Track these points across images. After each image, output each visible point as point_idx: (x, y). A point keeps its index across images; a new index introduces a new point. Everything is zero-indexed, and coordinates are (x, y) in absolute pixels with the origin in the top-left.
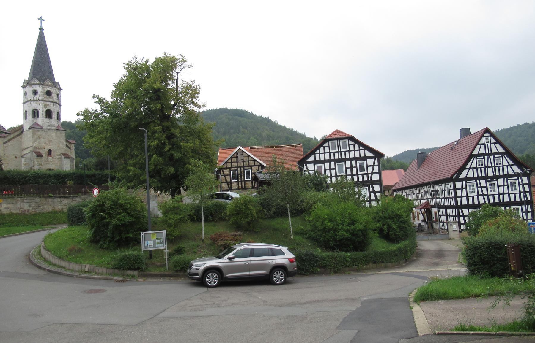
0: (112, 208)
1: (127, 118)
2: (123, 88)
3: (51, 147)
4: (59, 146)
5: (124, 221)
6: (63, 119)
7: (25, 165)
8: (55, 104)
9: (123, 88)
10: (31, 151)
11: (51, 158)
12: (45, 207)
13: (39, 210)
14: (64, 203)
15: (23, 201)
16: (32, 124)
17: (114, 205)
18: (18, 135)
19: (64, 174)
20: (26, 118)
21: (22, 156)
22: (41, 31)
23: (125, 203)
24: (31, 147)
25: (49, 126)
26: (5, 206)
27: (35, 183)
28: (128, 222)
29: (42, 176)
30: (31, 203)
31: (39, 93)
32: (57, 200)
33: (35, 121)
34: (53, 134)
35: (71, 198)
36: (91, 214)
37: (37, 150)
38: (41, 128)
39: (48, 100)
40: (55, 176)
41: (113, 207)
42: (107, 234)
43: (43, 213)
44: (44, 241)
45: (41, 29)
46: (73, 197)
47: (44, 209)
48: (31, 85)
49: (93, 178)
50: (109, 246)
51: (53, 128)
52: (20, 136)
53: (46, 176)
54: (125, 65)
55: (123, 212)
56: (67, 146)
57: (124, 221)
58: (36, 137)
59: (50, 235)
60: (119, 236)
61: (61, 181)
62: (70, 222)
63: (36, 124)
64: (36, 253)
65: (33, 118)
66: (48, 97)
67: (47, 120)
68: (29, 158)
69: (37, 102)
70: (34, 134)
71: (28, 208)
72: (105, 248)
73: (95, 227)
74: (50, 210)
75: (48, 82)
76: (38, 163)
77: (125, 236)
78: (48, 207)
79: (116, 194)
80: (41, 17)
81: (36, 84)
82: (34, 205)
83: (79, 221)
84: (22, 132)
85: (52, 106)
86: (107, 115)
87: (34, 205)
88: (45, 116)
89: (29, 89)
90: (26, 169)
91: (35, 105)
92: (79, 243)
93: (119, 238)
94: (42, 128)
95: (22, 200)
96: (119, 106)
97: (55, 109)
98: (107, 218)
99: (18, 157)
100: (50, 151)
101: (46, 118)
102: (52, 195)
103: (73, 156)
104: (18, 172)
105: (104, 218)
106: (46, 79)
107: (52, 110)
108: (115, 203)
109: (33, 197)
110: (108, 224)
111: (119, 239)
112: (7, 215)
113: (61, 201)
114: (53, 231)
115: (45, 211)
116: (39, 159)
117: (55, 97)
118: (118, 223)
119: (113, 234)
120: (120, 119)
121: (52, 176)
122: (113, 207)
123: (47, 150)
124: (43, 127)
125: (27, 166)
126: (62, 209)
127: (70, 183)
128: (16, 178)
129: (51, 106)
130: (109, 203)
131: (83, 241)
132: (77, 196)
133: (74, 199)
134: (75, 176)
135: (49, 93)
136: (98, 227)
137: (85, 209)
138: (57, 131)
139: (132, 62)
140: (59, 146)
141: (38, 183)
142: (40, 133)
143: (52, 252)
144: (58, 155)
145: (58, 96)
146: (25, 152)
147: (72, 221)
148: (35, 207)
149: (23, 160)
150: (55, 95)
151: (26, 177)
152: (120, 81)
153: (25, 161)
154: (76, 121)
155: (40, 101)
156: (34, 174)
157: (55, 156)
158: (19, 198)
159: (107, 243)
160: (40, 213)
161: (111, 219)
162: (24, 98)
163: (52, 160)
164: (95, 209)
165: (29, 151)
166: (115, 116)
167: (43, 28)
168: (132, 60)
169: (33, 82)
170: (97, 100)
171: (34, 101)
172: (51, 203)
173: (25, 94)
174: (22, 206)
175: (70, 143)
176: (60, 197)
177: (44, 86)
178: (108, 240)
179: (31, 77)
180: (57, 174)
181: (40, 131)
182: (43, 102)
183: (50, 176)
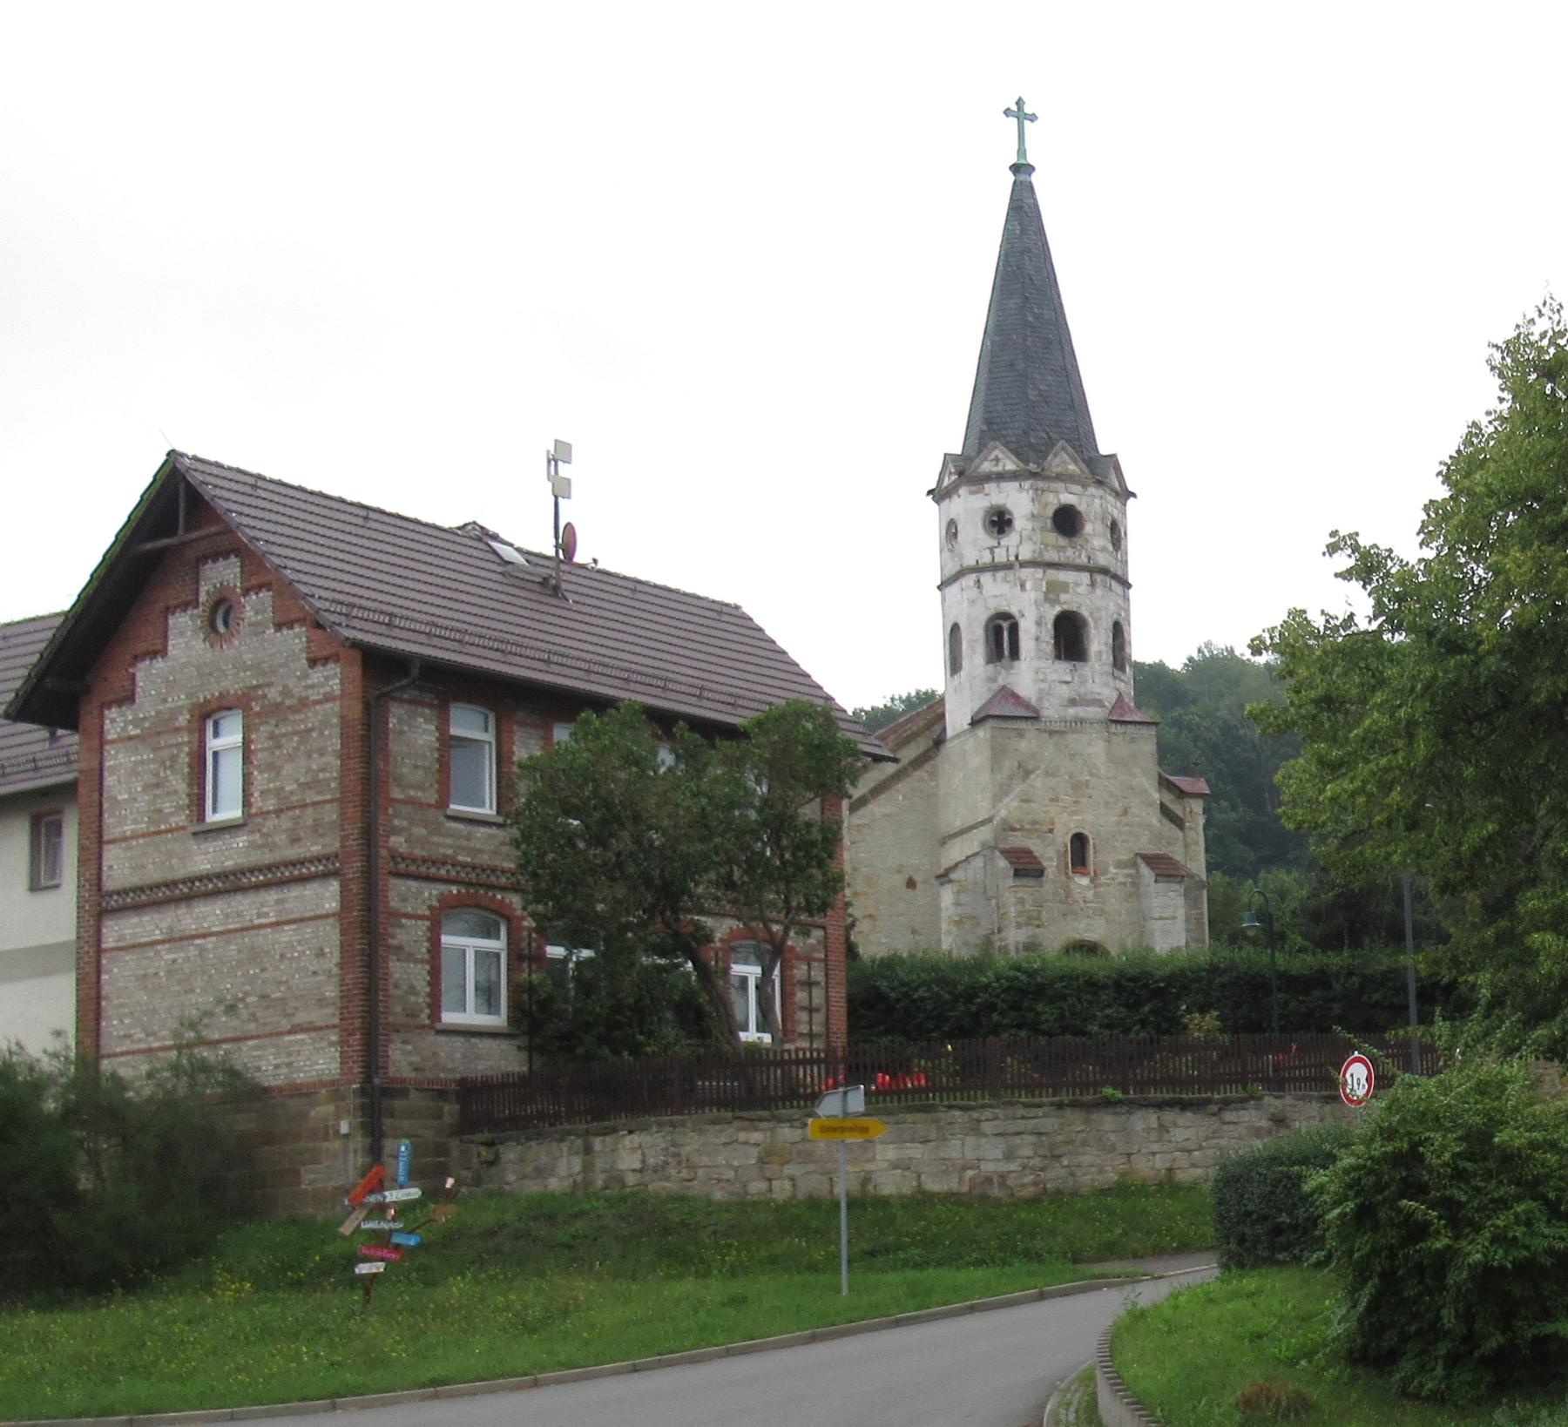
0: (1460, 1175)
1: (1507, 653)
2: (1487, 485)
3: (1089, 820)
4: (1125, 812)
5: (1527, 1248)
6: (1142, 650)
7: (959, 923)
8: (1099, 578)
9: (1487, 485)
10: (984, 845)
11: (1085, 881)
12: (1085, 1159)
13: (1055, 1176)
14: (1179, 1135)
15: (975, 1129)
16: (988, 696)
17: (1471, 1157)
18: (918, 763)
19: (1168, 970)
20: (954, 664)
21: (944, 877)
22: (1022, 177)
23: (1534, 1145)
24: (983, 823)
25: (1073, 702)
26: (890, 1153)
27: (1019, 1027)
28: (1550, 1252)
29: (1052, 983)
30: (1017, 1140)
31: (1020, 523)
32: (1144, 1121)
33: (1001, 682)
34: (1095, 747)
35: (1214, 1108)
36: (1351, 1205)
37: (1017, 841)
38: (1034, 716)
39: (1063, 560)
40: (1118, 985)
41: (1468, 1165)
42: (1439, 1318)
43: (1075, 1194)
44: (1113, 1343)
45: (1021, 169)
46: (1226, 1104)
47: (1079, 1173)
48: (979, 481)
49: (1316, 993)
50: (1449, 1388)
51: (1092, 712)
52: (928, 766)
53: (1075, 983)
54: (1498, 355)
55: (1519, 1199)
56: (1165, 810)
57: (1527, 1248)
58: (1009, 764)
59: (1139, 1316)
60: (1503, 1333)
61: (1152, 1011)
62: (1233, 1246)
63: (1007, 694)
64: (1072, 1417)
65: (989, 661)
66: (1063, 541)
67: (1063, 669)
68: (975, 883)
69: (1010, 575)
70: (997, 754)
71: (1004, 1167)
72: (1427, 1399)
73: (1376, 1280)
74: (1112, 1177)
75: (1063, 461)
76: (1020, 914)
77: (1535, 1331)
78: (1098, 1161)
79: (1482, 1093)
80: (1020, 102)
81: (1001, 477)
82: (1028, 1152)
83: (1282, 1239)
84: (939, 742)
85: (1082, 589)
86: (1399, 638)
87: (1028, 1152)
88: (1049, 648)
89: (970, 506)
90: (966, 944)
91: (999, 593)
92: (1292, 1362)
93: (1501, 1339)
94: (1035, 718)
95: (972, 1119)
96: (1462, 584)
97: (1099, 609)
98: (1438, 1232)
99: (918, 878)
100: (1079, 841)
101: (1058, 657)
102: (1119, 1095)
103: (1198, 864)
104: (935, 968)
105: (1417, 1231)
106: (1050, 444)
107: (1085, 613)
108: (1478, 1141)
109: (1026, 1106)
110: (1443, 1261)
111: (1501, 1348)
112: (903, 1207)
113: (1163, 1129)
114: (1149, 1294)
115: (1088, 1180)
116: (1027, 891)
117: (1098, 542)
118: (1499, 1257)
119: (1467, 1316)
120: (1476, 663)
121: (1105, 987)
122: (1468, 1165)
123: (1063, 838)
124: (1045, 713)
125: (967, 927)
126: (1170, 1170)
127: (1202, 1025)
128: (922, 999)
129: (1080, 590)
130: (1444, 1148)
131: (1309, 1355)
132: (1243, 1101)
133: (1229, 1116)
134: (1223, 986)
135: (1067, 522)
136: (1388, 1276)
137: (1316, 1179)
138: (1113, 728)
139: (1533, 329)
140: (1125, 812)
141: (1035, 1029)
142: (1028, 743)
143: (1159, 1413)
144: (1120, 865)
145: (1116, 533)
146: (956, 851)
147: (1242, 1240)
148: (1037, 1162)
149: (947, 896)
150: (1100, 528)
151: (970, 994)
152: (1468, 441)
153: (957, 904)
154: (1191, 659)
155: (1023, 564)
156: (1012, 973)
157: (1106, 872)
158: (957, 1113)
159: (1439, 1371)
160: (1059, 1192)
161: (1457, 1238)
162: (947, 554)
163: (1090, 895)
164: (1372, 1179)
165: (976, 849)
166: (1453, 644)
167: (1031, 160)
168: (1532, 321)
169: (987, 467)
170: (1351, 562)
171: (994, 568)
172: (1112, 1137)
173: (951, 531)
174: (970, 1155)
175: (1181, 794)
176: (1160, 1106)
177: (1041, 484)
178: (1443, 1352)
179: (973, 440)
180: (1131, 972)
181: (1028, 735)
182: (1039, 573)
183: (1093, 985)
